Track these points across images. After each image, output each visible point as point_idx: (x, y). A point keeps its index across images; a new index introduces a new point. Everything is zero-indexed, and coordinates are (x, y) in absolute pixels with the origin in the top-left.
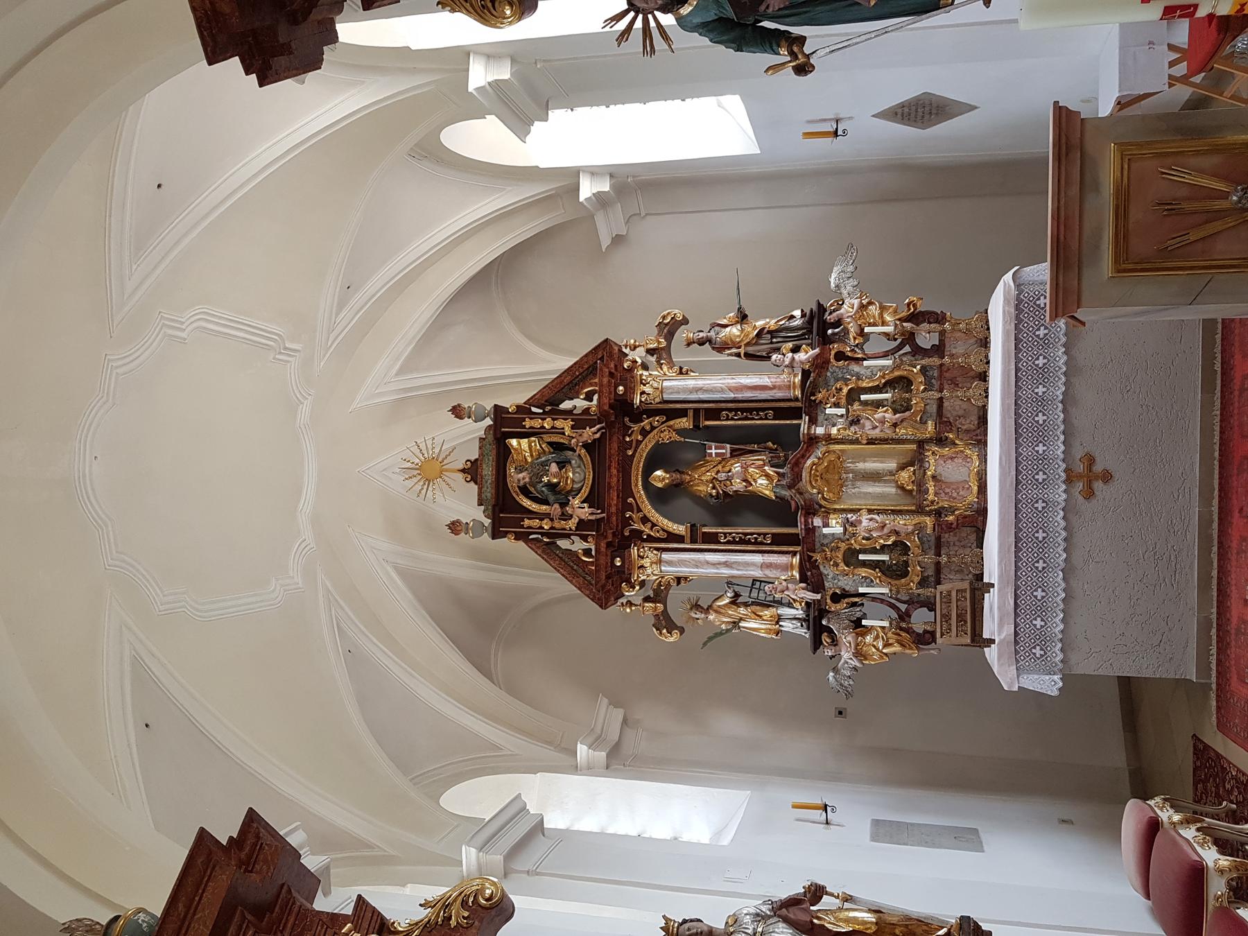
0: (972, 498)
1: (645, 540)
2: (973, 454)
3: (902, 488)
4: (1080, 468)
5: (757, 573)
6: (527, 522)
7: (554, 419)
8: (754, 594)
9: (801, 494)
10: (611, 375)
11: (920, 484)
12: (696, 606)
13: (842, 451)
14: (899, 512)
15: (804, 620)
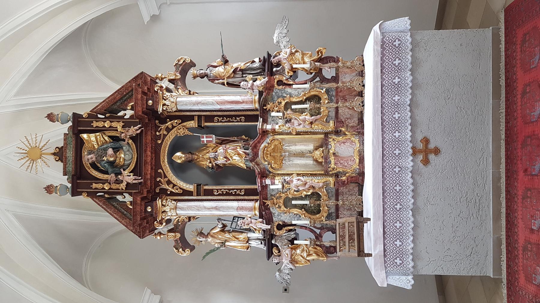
0: (356, 166)
1: (169, 195)
2: (356, 140)
3: (316, 161)
4: (420, 146)
5: (236, 213)
6: (94, 186)
7: (111, 122)
8: (234, 226)
9: (258, 165)
10: (144, 93)
11: (326, 158)
12: (201, 234)
13: (282, 139)
14: (315, 175)
15: (263, 240)
